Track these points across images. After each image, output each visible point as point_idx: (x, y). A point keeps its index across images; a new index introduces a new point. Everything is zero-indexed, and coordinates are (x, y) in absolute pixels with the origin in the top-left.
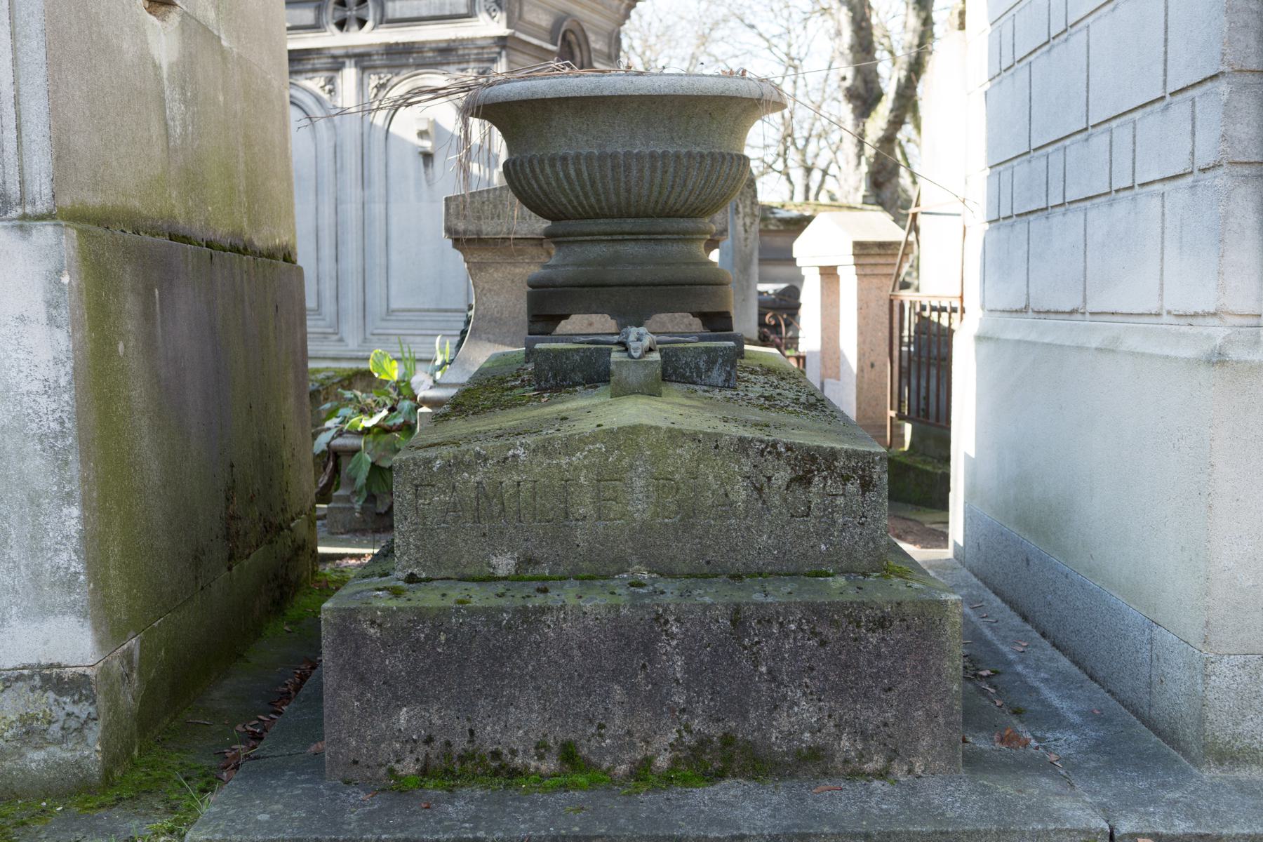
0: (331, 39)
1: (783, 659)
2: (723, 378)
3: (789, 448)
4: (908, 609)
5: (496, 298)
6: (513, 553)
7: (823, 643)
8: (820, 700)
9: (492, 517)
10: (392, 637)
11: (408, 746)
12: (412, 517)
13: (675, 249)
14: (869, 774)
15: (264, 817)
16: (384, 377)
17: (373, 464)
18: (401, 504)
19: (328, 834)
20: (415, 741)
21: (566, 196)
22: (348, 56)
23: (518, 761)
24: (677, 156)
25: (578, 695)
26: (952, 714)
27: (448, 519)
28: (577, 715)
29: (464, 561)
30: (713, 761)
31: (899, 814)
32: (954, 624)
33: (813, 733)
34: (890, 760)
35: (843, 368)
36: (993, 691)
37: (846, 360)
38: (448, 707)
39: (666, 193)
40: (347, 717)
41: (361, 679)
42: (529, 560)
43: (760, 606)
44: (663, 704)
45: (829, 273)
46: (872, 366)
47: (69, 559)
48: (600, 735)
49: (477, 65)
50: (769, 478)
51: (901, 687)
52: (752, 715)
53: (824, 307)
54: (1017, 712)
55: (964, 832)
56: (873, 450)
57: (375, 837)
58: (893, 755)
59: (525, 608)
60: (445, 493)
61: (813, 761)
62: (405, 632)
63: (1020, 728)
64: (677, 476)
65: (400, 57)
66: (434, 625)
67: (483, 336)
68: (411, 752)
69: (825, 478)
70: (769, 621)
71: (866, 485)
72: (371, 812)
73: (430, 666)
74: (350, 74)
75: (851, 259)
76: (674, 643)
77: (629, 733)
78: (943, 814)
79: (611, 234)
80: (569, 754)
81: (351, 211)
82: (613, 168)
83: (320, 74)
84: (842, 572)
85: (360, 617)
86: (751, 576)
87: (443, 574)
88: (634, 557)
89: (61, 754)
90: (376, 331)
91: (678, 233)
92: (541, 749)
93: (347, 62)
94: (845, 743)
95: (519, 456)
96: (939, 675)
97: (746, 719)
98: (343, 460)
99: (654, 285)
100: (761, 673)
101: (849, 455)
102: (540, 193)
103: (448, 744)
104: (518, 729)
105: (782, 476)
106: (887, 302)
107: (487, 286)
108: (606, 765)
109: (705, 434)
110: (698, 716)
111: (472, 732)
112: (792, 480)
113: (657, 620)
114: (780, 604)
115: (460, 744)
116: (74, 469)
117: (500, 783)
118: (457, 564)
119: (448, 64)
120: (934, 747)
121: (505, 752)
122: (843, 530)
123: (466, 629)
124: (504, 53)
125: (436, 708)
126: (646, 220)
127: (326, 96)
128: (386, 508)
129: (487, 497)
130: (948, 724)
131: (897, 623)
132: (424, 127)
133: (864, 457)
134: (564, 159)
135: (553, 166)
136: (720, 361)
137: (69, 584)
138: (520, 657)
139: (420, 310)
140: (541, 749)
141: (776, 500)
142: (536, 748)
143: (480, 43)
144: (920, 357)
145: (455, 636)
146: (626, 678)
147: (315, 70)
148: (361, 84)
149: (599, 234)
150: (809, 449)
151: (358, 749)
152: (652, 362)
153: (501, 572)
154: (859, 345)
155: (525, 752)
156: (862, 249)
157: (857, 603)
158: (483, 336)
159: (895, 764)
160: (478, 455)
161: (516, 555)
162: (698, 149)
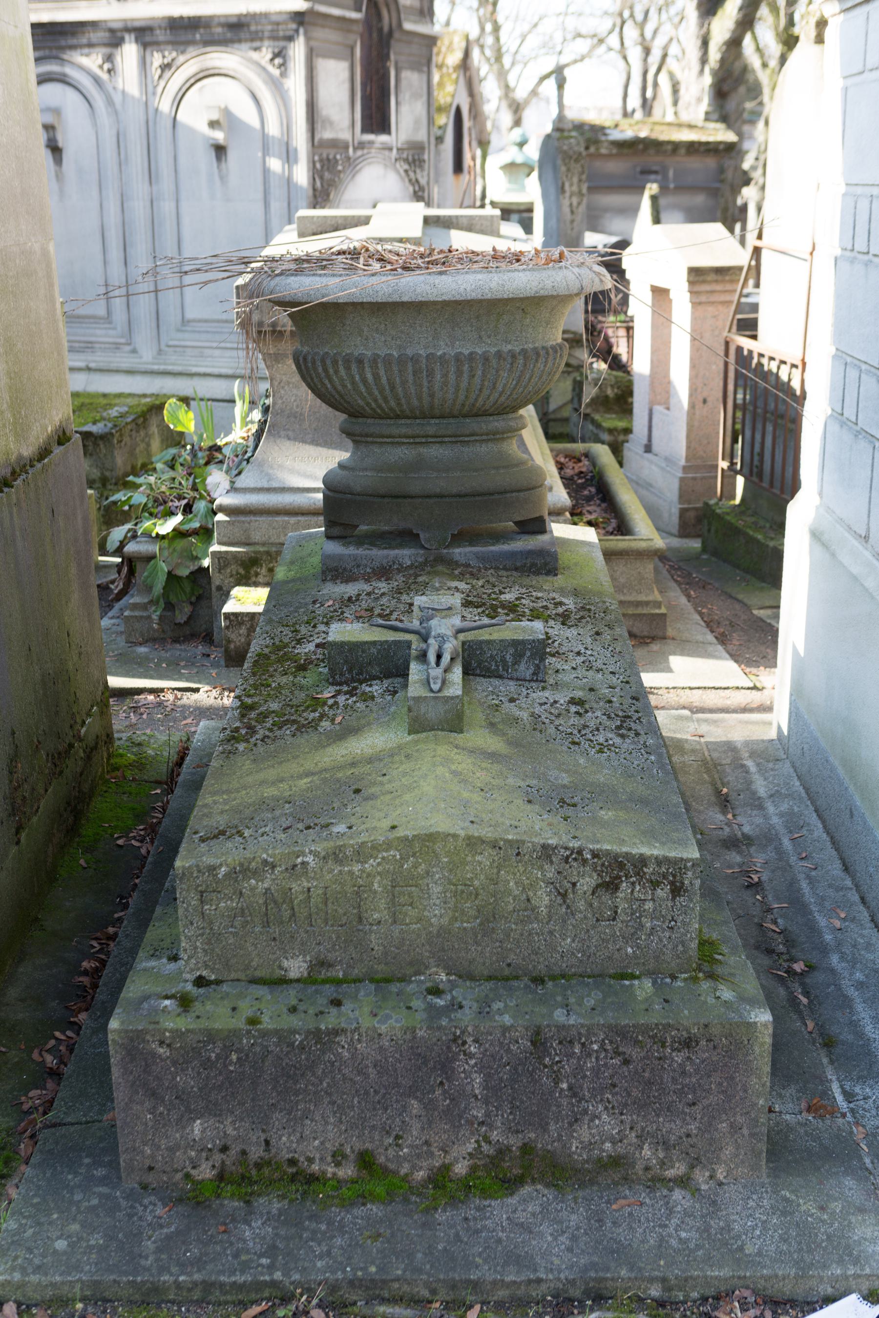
1: (585, 1076)
2: (531, 671)
3: (595, 855)
4: (715, 1030)
5: (295, 391)
6: (305, 956)
7: (626, 1062)
8: (622, 1114)
9: (282, 922)
10: (183, 1056)
11: (204, 1154)
12: (198, 922)
13: (483, 449)
14: (670, 1180)
15: (61, 1245)
16: (179, 429)
17: (169, 573)
18: (186, 910)
19: (126, 1273)
20: (210, 1150)
21: (364, 399)
22: (128, 30)
23: (315, 1167)
24: (486, 359)
25: (374, 1109)
26: (757, 1126)
27: (236, 923)
28: (373, 1127)
29: (254, 964)
31: (698, 1247)
32: (762, 1044)
33: (614, 1143)
34: (692, 1167)
35: (672, 401)
36: (805, 1001)
37: (676, 393)
38: (242, 1120)
39: (473, 396)
40: (140, 1128)
41: (153, 1094)
42: (322, 963)
43: (561, 1028)
44: (461, 1117)
45: (660, 294)
46: (705, 401)
48: (397, 1145)
49: (271, 43)
50: (574, 884)
51: (706, 1102)
52: (552, 1127)
53: (655, 327)
54: (829, 1044)
55: (762, 1277)
56: (685, 855)
57: (172, 1279)
58: (695, 1162)
59: (318, 1030)
60: (231, 899)
62: (193, 1051)
63: (830, 1074)
64: (476, 883)
66: (225, 1046)
67: (282, 433)
68: (207, 1159)
69: (633, 884)
70: (570, 1042)
71: (677, 890)
72: (169, 1237)
73: (223, 1083)
74: (130, 51)
75: (686, 285)
76: (472, 1062)
77: (427, 1143)
78: (741, 1249)
79: (413, 437)
80: (365, 1161)
81: (139, 208)
82: (415, 373)
83: (97, 49)
84: (649, 973)
85: (148, 1037)
86: (553, 978)
87: (233, 976)
88: (431, 960)
90: (171, 343)
91: (487, 434)
92: (338, 1157)
93: (127, 37)
94: (647, 1152)
95: (308, 863)
96: (745, 1091)
97: (545, 1130)
98: (139, 567)
99: (460, 496)
100: (562, 1090)
101: (659, 861)
102: (334, 393)
103: (244, 1153)
104: (316, 1140)
105: (587, 882)
106: (723, 343)
107: (284, 378)
108: (403, 1172)
109: (507, 841)
110: (496, 1129)
111: (267, 1143)
112: (598, 886)
113: (455, 1040)
114: (582, 1026)
115: (256, 1153)
117: (297, 1190)
118: (247, 967)
119: (240, 41)
120: (737, 1156)
121: (302, 1159)
122: (651, 934)
123: (258, 1049)
124: (301, 31)
125: (230, 1120)
126: (452, 420)
127: (105, 76)
128: (185, 619)
129: (275, 902)
130: (752, 1135)
131: (703, 1043)
132: (215, 116)
133: (675, 864)
134: (360, 362)
135: (348, 368)
136: (528, 654)
138: (314, 1074)
139: (218, 321)
140: (338, 1157)
141: (581, 905)
142: (333, 1156)
143: (274, 18)
144: (755, 407)
145: (247, 1055)
146: (424, 1094)
147: (91, 45)
148: (143, 64)
149: (400, 437)
150: (616, 856)
151: (153, 1156)
152: (452, 698)
153: (293, 974)
154: (690, 379)
155: (321, 1159)
156: (697, 275)
157: (663, 1025)
158: (282, 433)
159: (697, 1171)
160: (265, 862)
161: (308, 958)
162: (509, 347)
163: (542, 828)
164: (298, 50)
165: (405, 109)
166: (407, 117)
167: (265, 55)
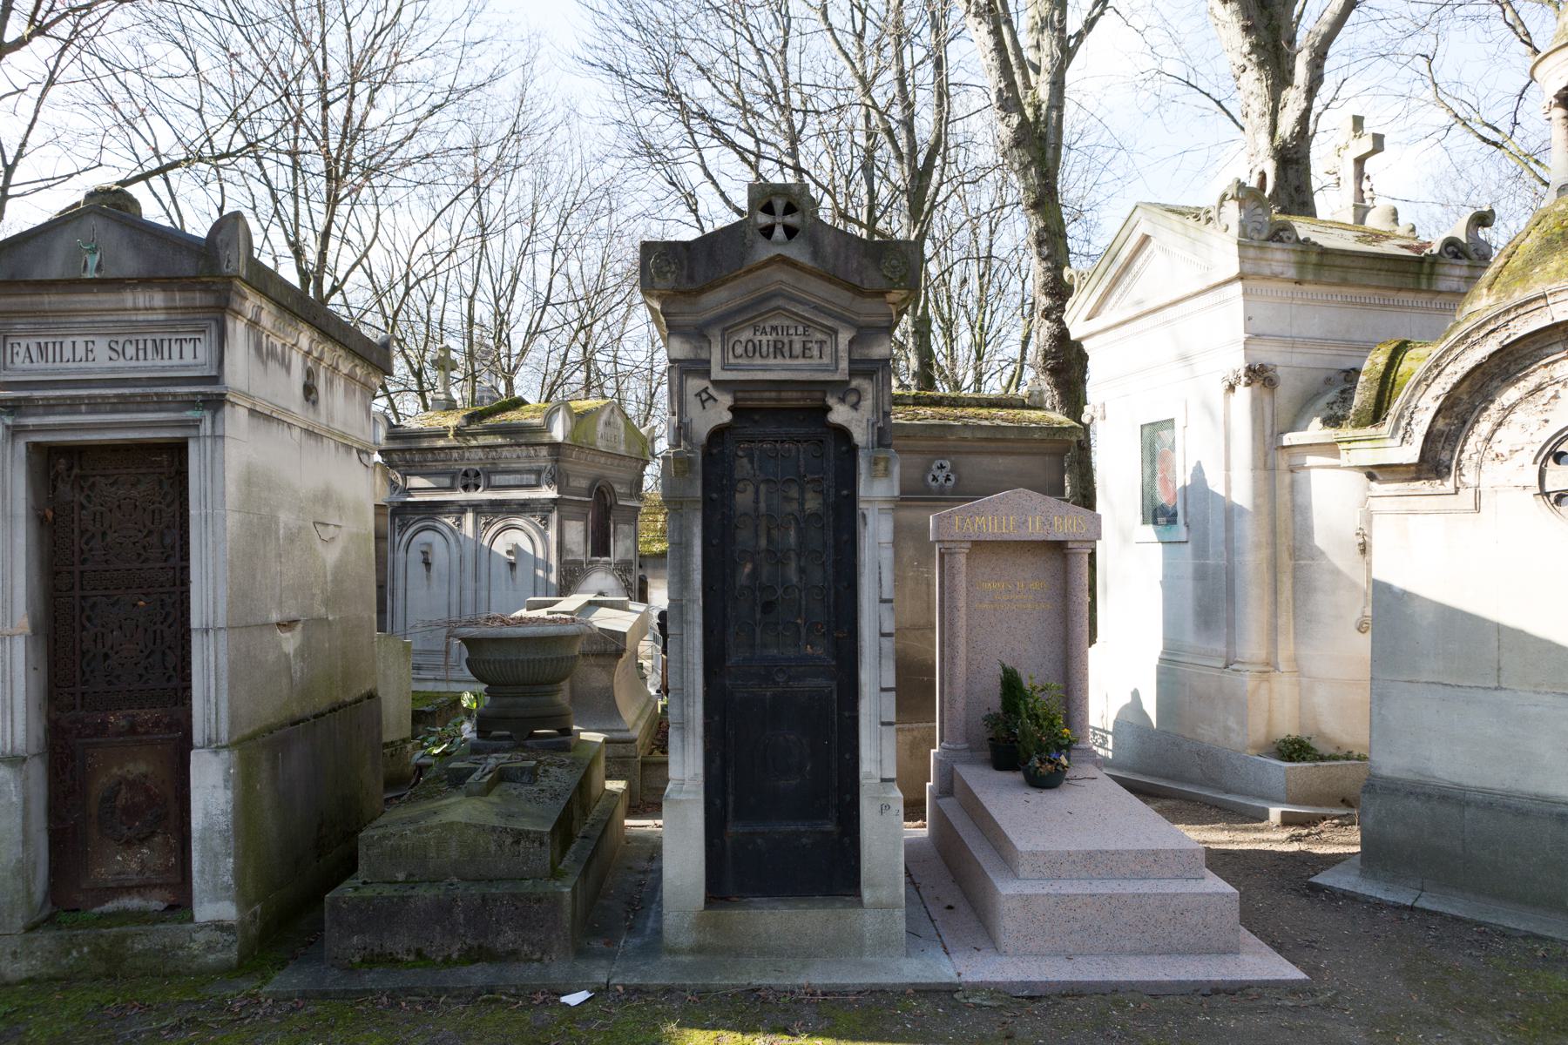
0: (460, 496)
30: (475, 955)
42: (411, 875)
47: (228, 879)
61: (513, 955)
65: (498, 508)
71: (542, 844)
74: (469, 518)
80: (419, 953)
89: (221, 956)
92: (409, 951)
104: (400, 944)
105: (509, 841)
116: (232, 844)
137: (228, 888)
148: (476, 523)
163: (495, 821)
164: (554, 517)
165: (619, 544)
166: (620, 548)
167: (536, 520)
